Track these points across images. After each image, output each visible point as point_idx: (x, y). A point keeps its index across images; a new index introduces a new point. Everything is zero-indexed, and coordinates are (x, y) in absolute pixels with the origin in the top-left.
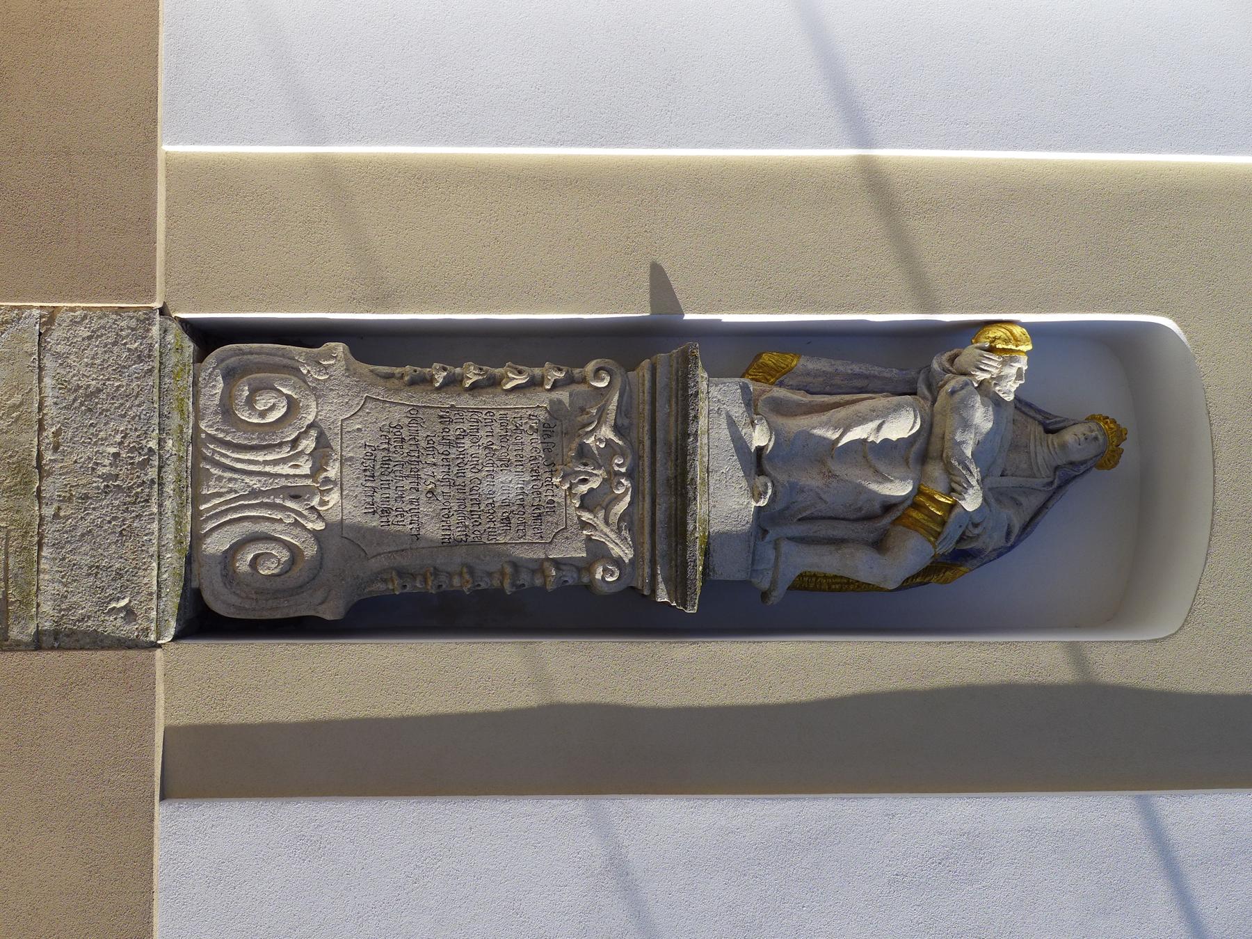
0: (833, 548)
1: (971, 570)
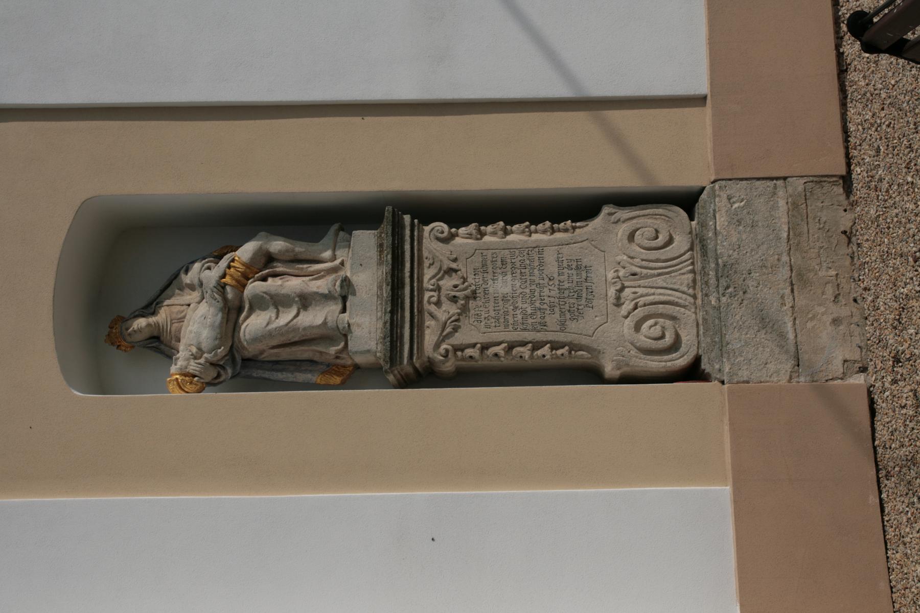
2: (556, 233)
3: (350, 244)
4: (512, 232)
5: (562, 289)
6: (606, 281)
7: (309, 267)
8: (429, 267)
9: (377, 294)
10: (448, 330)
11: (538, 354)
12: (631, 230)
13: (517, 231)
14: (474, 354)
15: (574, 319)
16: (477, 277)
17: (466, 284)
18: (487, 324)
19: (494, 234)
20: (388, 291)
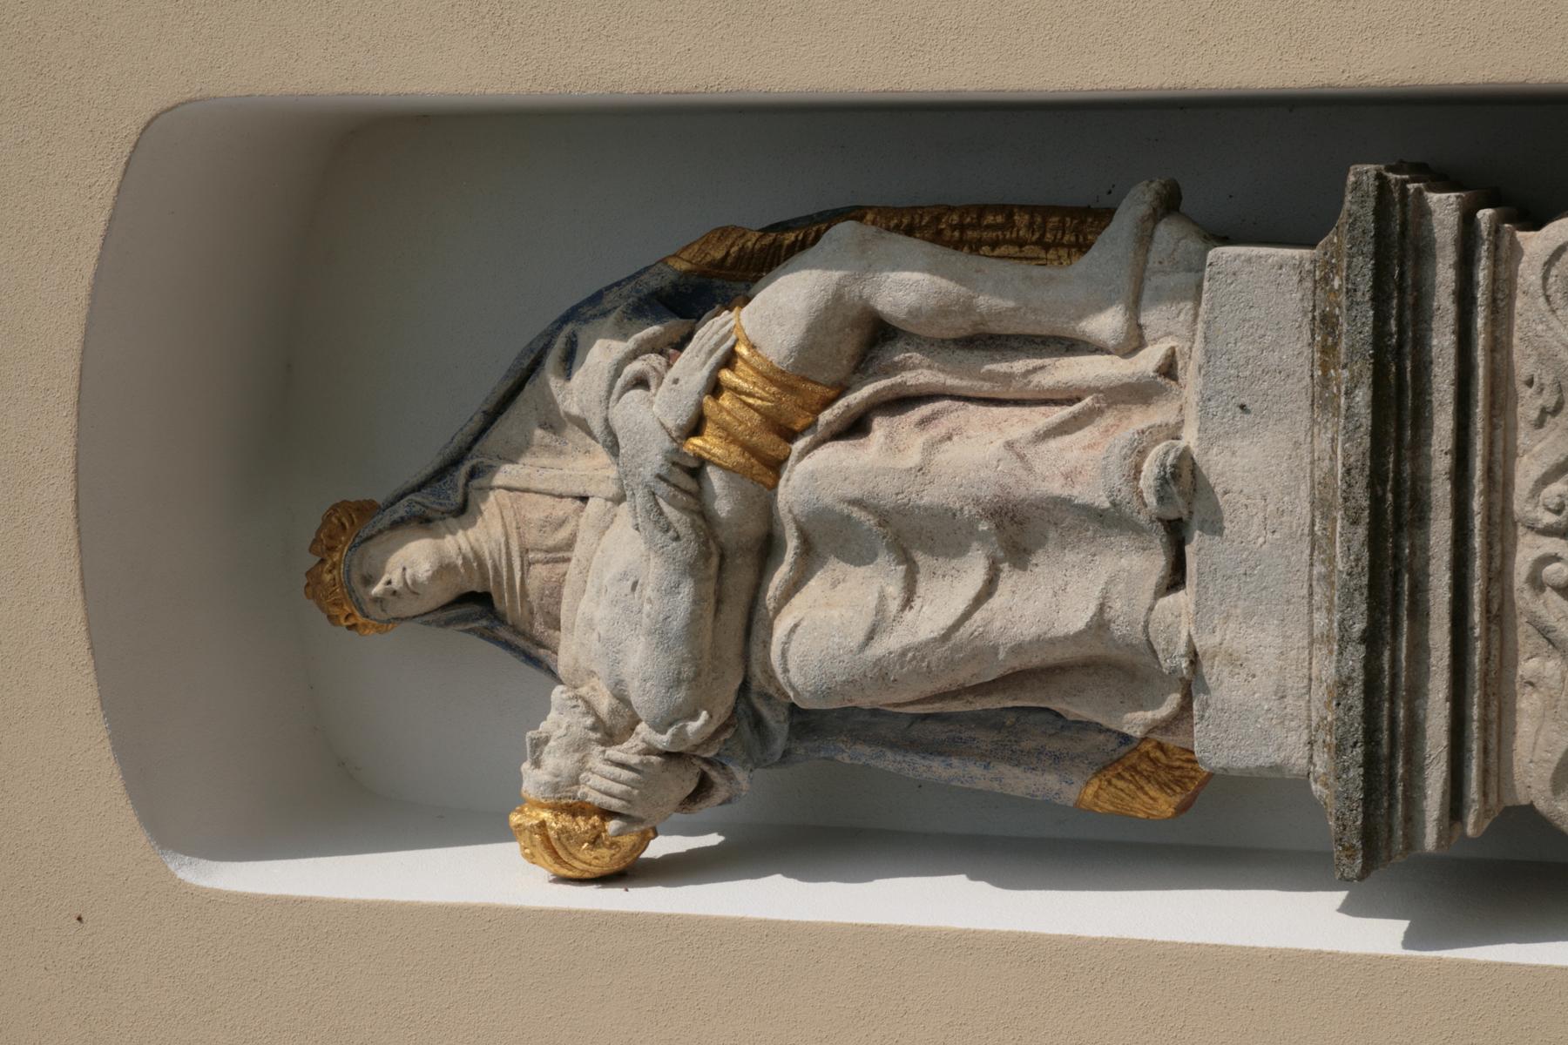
0: (995, 328)
1: (664, 261)
3: (1199, 286)
7: (1035, 370)
8: (1540, 423)
9: (1312, 532)
20: (1356, 546)
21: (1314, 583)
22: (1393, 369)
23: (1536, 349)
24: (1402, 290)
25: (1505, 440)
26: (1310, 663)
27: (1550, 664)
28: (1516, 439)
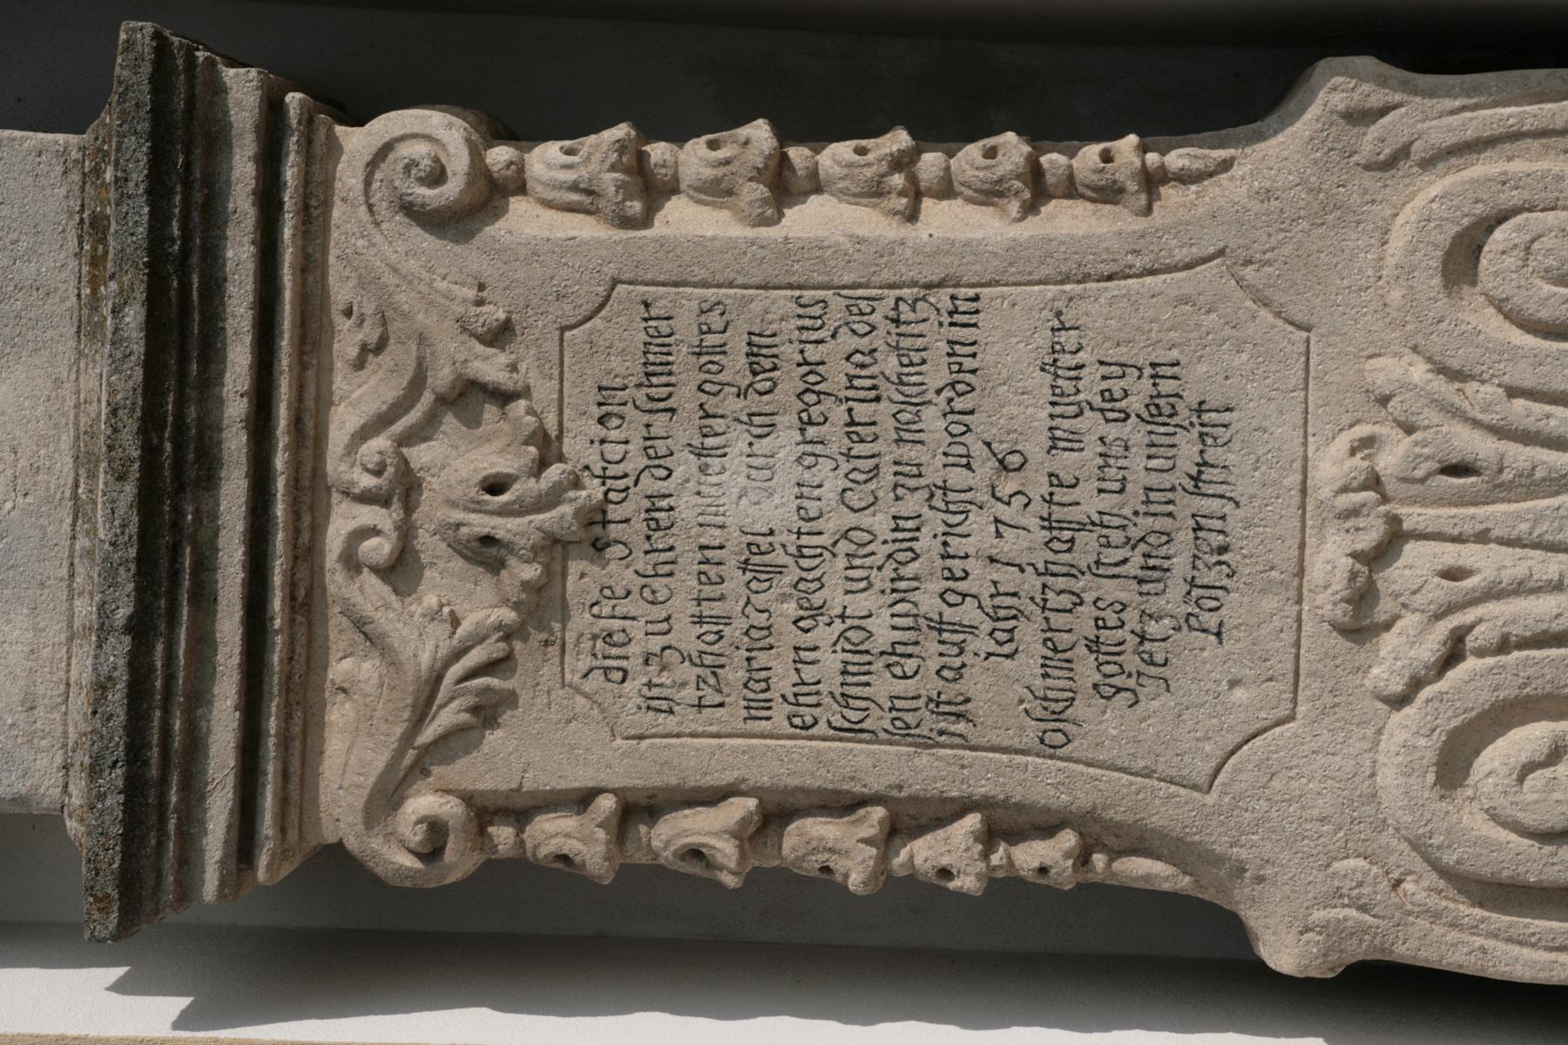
2: (1054, 202)
4: (816, 185)
5: (1062, 525)
6: (1304, 491)
8: (360, 364)
9: (75, 496)
10: (447, 717)
11: (918, 861)
12: (1466, 222)
13: (841, 185)
14: (578, 846)
15: (1119, 690)
16: (614, 435)
17: (554, 472)
18: (655, 692)
19: (717, 191)
20: (122, 508)
21: (77, 561)
22: (175, 284)
23: (356, 270)
24: (187, 186)
25: (318, 383)
26: (69, 665)
27: (367, 665)
28: (331, 383)
